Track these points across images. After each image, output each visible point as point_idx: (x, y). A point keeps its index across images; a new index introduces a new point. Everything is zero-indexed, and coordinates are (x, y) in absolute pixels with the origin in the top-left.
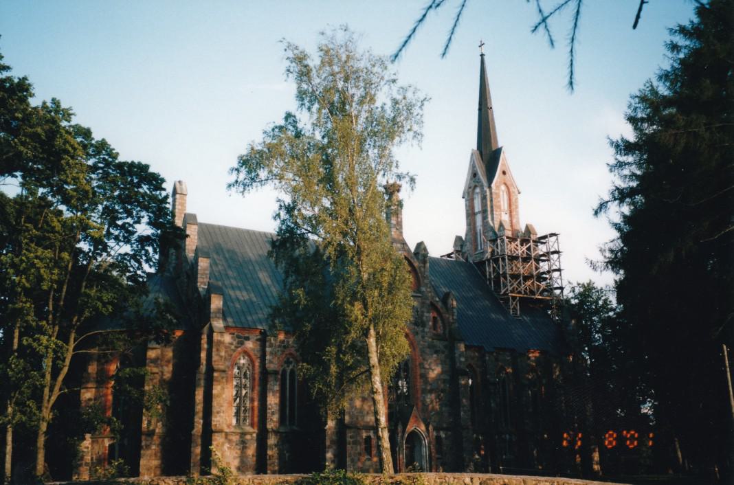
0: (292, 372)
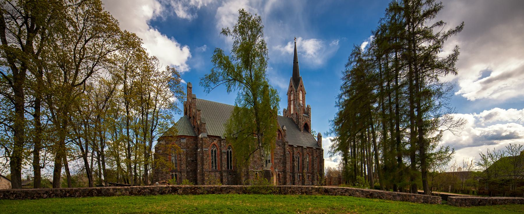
0: (231, 152)
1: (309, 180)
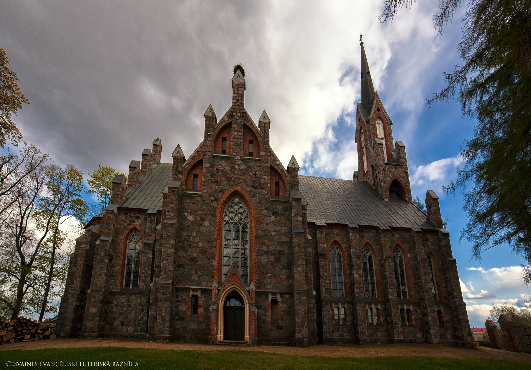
1: (410, 325)
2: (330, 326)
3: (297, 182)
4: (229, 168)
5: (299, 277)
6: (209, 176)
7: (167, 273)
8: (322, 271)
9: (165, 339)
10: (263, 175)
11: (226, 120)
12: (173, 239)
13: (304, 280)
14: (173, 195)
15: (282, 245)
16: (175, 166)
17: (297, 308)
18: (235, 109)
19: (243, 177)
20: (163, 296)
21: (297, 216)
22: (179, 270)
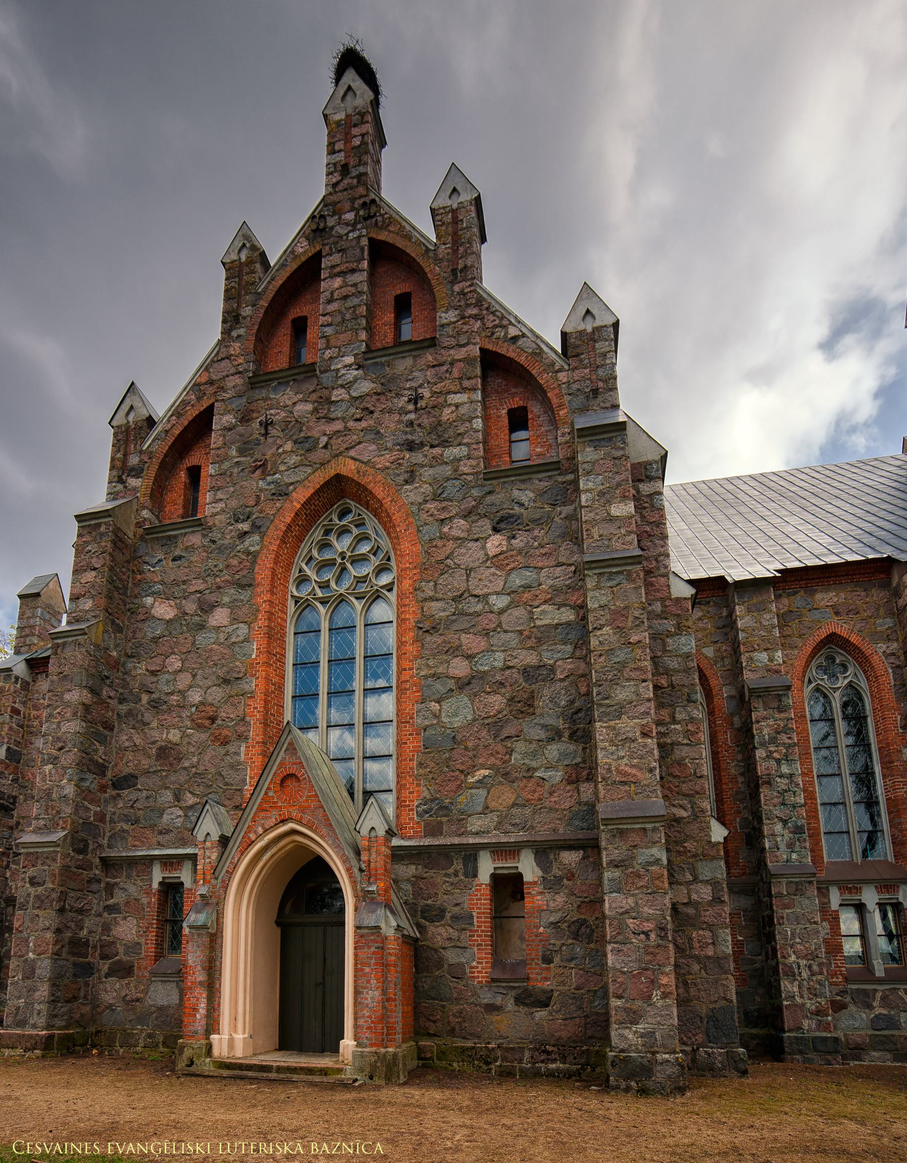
2: (820, 983)
3: (605, 381)
4: (309, 407)
5: (625, 761)
6: (234, 453)
7: (53, 809)
8: (769, 756)
9: (28, 1045)
10: (449, 393)
11: (301, 250)
12: (80, 686)
13: (651, 770)
14: (95, 540)
15: (539, 641)
16: (119, 455)
17: (612, 903)
18: (334, 204)
19: (364, 424)
20: (32, 890)
21: (609, 502)
22: (119, 795)
